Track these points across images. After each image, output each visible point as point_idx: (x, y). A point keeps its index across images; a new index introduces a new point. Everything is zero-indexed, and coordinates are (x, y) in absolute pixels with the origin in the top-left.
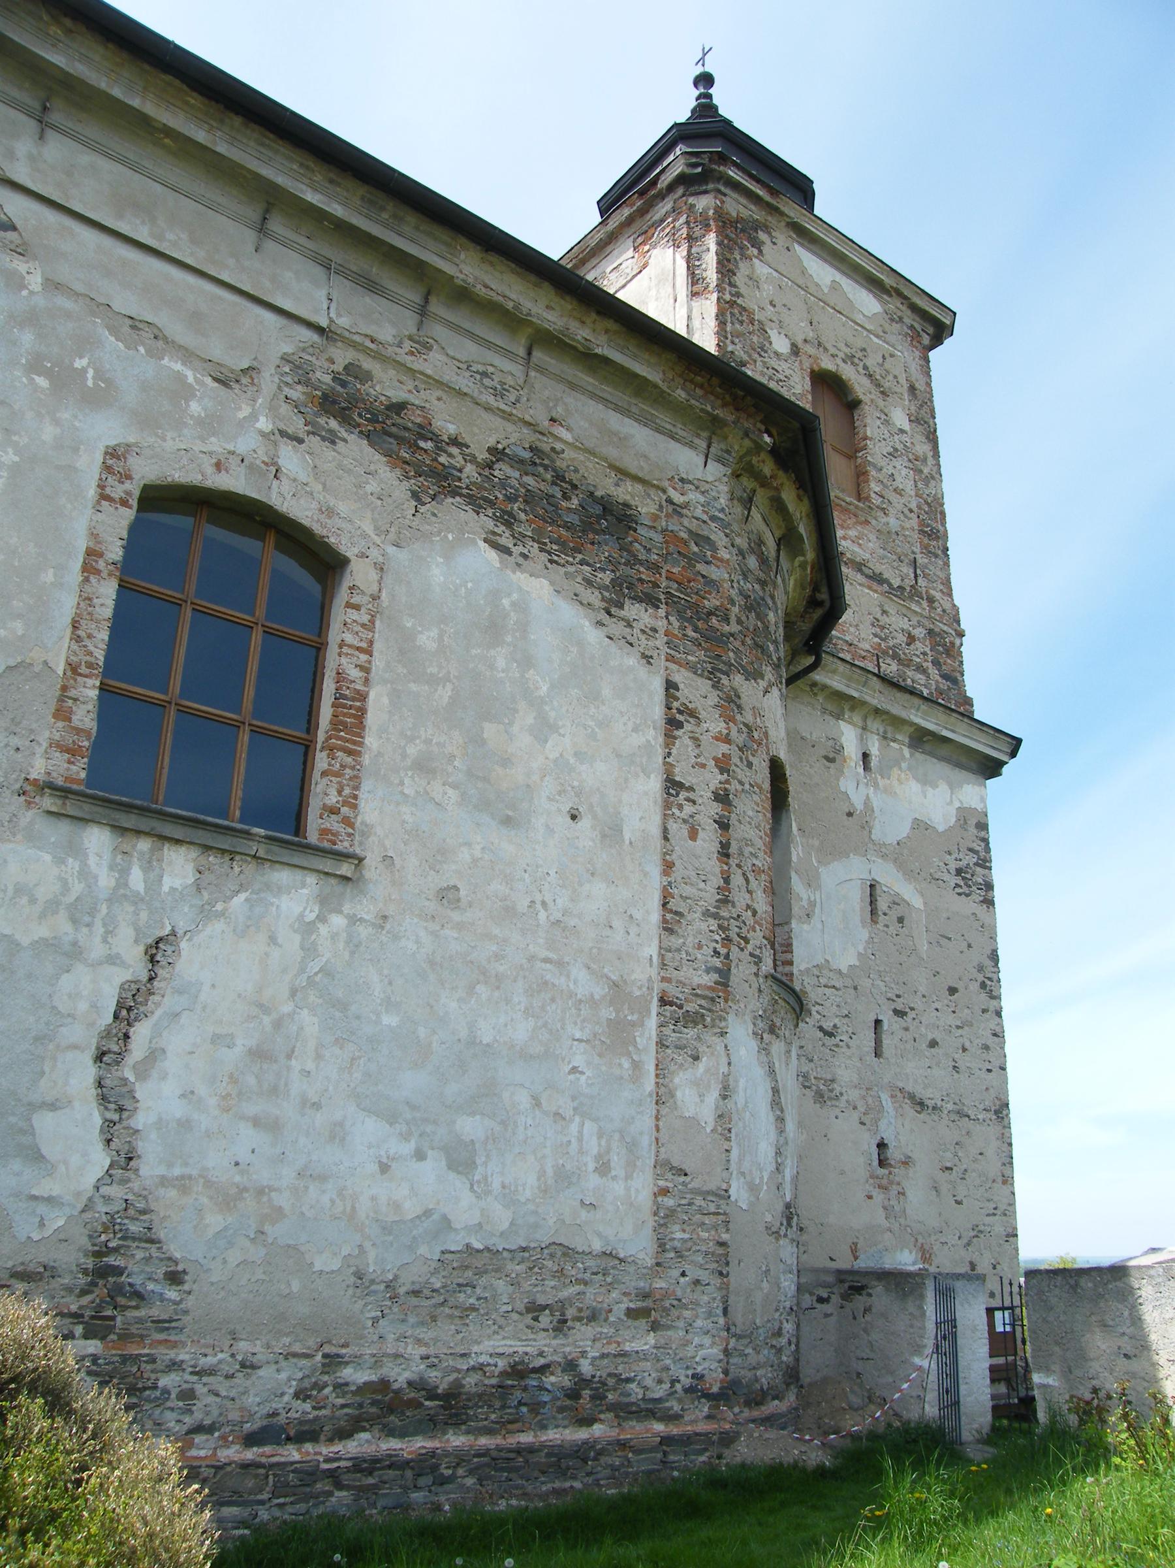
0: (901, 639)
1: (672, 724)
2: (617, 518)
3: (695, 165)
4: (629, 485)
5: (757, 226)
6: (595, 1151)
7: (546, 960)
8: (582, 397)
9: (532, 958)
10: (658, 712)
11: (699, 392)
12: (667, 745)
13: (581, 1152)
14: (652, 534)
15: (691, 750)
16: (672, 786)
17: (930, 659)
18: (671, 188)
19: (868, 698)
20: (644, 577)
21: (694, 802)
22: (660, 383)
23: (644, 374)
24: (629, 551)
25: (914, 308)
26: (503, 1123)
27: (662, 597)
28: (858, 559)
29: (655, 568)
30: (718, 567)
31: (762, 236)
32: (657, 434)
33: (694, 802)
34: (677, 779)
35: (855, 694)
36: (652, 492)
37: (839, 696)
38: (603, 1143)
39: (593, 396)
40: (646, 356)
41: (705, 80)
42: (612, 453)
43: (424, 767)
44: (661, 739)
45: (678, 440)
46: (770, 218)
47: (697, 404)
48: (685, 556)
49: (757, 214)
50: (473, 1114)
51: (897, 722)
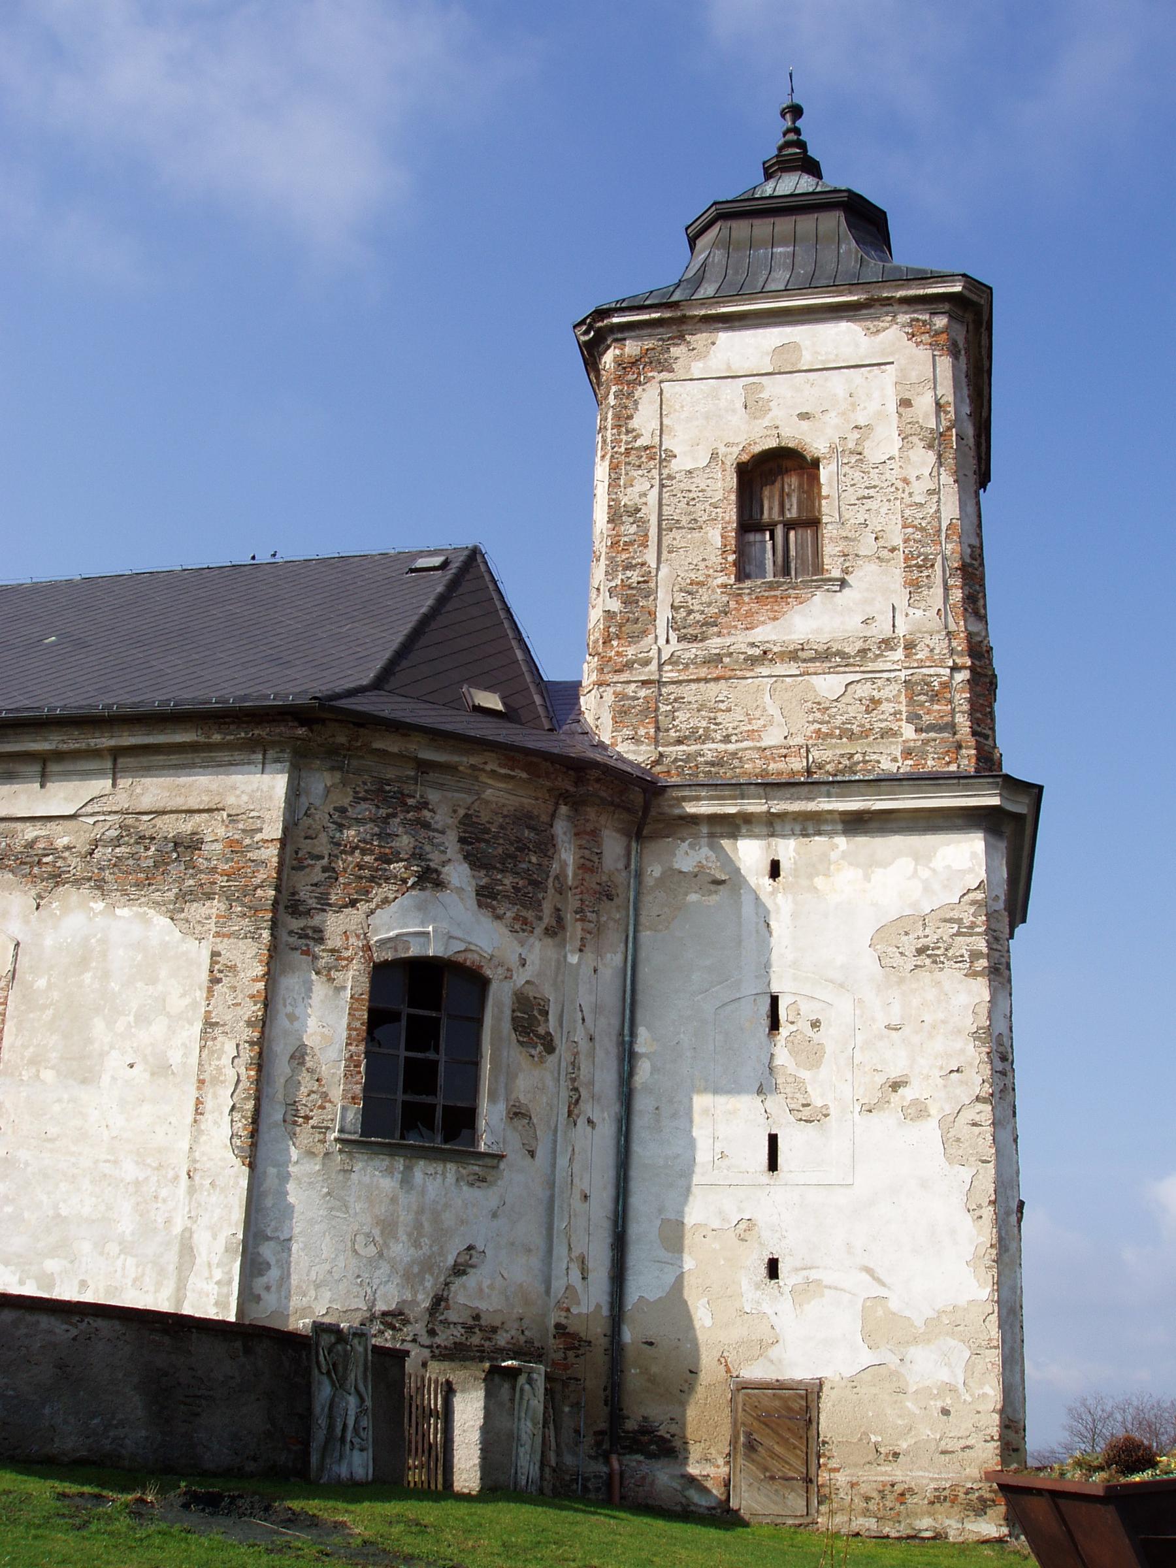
0: (855, 710)
1: (215, 981)
4: (197, 818)
6: (134, 1276)
7: (107, 1161)
9: (96, 1162)
10: (204, 976)
11: (232, 727)
13: (123, 1276)
16: (209, 1024)
26: (72, 1262)
28: (791, 648)
29: (214, 870)
37: (713, 819)
38: (140, 1270)
41: (796, 111)
43: (34, 1061)
45: (237, 765)
50: (53, 1258)
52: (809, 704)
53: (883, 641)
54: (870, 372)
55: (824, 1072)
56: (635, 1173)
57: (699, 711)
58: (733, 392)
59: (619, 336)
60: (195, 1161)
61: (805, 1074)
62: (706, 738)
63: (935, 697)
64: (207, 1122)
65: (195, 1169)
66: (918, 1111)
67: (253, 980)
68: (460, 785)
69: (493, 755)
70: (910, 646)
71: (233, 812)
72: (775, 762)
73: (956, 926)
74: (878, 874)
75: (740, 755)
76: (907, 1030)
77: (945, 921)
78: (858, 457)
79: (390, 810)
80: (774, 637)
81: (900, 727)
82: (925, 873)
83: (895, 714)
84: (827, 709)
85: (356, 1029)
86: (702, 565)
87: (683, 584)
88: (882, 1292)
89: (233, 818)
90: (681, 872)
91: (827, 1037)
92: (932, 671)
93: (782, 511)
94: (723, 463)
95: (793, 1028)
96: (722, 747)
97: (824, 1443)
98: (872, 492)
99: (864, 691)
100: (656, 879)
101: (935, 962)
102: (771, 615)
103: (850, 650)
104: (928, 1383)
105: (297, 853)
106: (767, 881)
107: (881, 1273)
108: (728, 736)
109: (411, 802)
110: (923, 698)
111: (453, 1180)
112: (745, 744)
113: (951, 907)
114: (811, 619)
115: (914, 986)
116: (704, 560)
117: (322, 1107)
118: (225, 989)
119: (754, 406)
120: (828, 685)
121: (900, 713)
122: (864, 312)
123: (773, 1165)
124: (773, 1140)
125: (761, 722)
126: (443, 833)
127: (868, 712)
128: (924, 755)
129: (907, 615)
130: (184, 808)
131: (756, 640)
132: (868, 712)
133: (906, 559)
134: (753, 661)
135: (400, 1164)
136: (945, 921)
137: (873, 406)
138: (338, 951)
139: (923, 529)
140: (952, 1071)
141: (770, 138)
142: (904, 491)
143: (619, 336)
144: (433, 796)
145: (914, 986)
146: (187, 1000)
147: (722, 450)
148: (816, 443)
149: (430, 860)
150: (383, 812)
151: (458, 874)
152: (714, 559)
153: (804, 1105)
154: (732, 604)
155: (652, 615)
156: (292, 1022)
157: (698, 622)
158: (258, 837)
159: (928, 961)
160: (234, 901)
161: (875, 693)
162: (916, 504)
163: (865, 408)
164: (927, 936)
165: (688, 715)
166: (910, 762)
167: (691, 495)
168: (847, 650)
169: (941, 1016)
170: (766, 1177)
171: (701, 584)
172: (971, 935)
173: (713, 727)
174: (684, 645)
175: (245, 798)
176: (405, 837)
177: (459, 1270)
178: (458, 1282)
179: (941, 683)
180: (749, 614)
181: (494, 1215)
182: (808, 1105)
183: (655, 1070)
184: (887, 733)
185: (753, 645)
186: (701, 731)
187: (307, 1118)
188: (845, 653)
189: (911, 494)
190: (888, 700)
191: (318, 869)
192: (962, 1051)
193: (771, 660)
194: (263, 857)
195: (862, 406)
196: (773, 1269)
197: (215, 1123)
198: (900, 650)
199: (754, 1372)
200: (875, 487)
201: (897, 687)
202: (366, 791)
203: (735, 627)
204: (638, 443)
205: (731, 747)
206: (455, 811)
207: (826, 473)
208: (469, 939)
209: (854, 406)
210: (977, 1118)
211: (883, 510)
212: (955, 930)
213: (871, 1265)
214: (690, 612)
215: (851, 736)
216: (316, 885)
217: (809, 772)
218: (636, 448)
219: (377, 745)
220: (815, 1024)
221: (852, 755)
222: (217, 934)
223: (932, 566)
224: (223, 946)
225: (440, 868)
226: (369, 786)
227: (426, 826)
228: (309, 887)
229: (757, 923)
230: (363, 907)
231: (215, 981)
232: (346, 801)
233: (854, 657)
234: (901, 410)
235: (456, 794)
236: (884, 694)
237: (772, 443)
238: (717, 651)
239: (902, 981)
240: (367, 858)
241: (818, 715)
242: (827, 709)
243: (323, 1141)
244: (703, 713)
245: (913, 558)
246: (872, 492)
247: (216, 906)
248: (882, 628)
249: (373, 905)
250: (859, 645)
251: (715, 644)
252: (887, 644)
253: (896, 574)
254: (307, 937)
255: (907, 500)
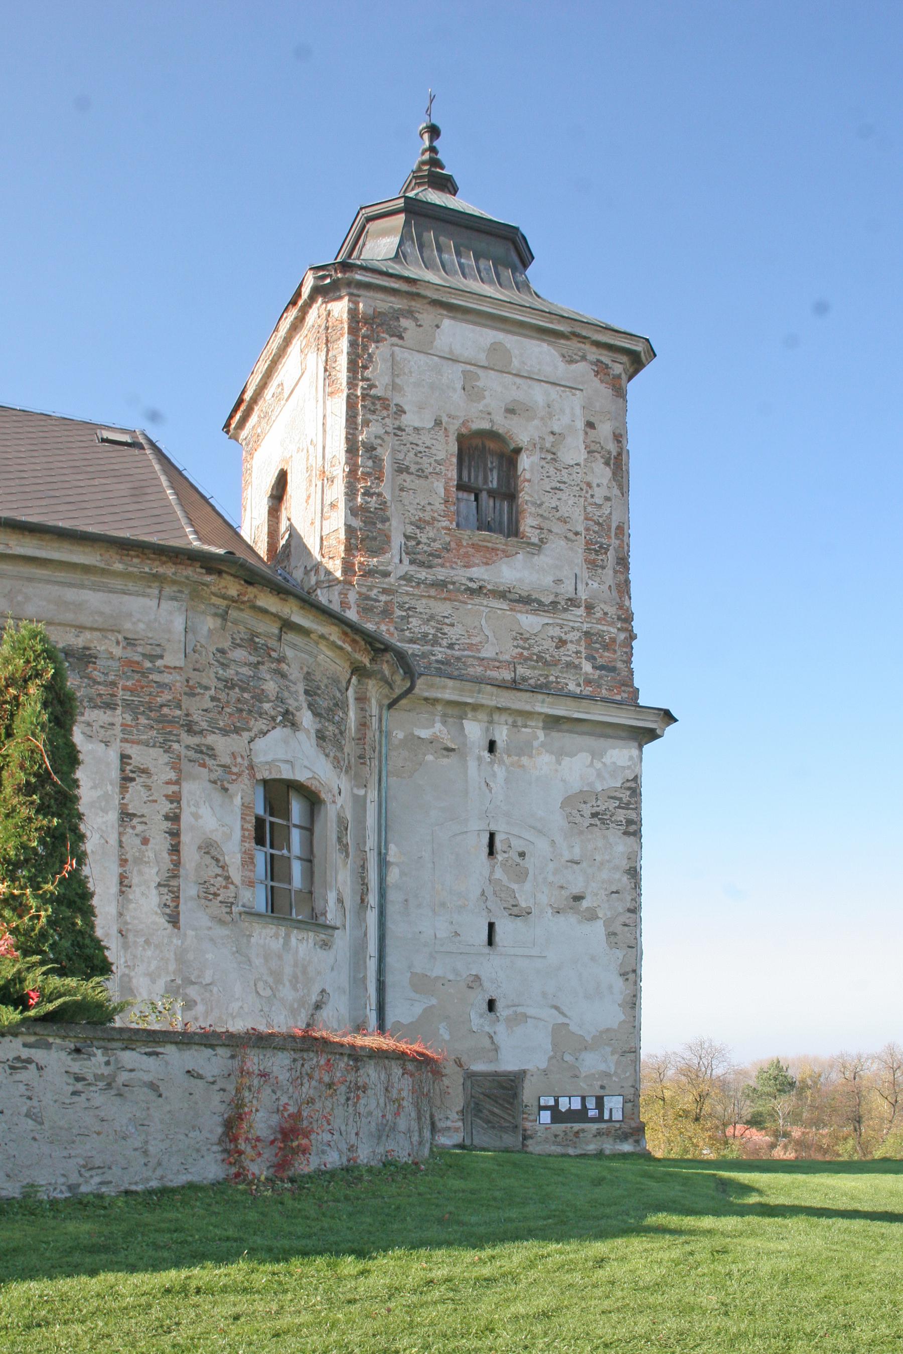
0: (549, 645)
1: (126, 780)
2: (78, 659)
3: (323, 277)
4: (88, 635)
5: (397, 315)
8: (40, 585)
10: (115, 774)
12: (121, 793)
14: (110, 662)
15: (144, 793)
16: (126, 816)
17: (583, 655)
18: (312, 299)
19: (484, 702)
20: (102, 692)
21: (146, 823)
22: (98, 564)
23: (82, 561)
24: (89, 678)
25: (598, 344)
27: (119, 702)
28: (501, 588)
29: (113, 684)
30: (171, 673)
31: (404, 322)
32: (110, 595)
33: (146, 823)
34: (130, 812)
35: (469, 700)
36: (109, 635)
39: (48, 582)
40: (81, 549)
42: (69, 617)
44: (117, 790)
45: (130, 594)
46: (413, 303)
47: (136, 569)
48: (138, 672)
49: (398, 303)
51: (528, 715)
52: (514, 633)
53: (569, 599)
54: (563, 391)
55: (528, 886)
56: (389, 942)
57: (428, 620)
58: (453, 374)
59: (355, 291)
60: (126, 923)
61: (515, 886)
62: (435, 642)
63: (606, 647)
64: (135, 894)
65: (128, 930)
66: (591, 916)
67: (167, 783)
68: (307, 647)
69: (337, 629)
70: (590, 608)
71: (129, 636)
72: (491, 670)
73: (618, 802)
74: (566, 761)
75: (463, 660)
76: (584, 865)
77: (612, 798)
78: (552, 456)
79: (260, 659)
80: (486, 577)
81: (580, 663)
82: (598, 765)
83: (577, 653)
84: (528, 639)
85: (248, 830)
86: (428, 508)
87: (413, 519)
88: (566, 1021)
89: (130, 642)
90: (420, 738)
91: (529, 863)
92: (605, 628)
93: (485, 481)
94: (446, 429)
95: (506, 855)
96: (449, 652)
97: (526, 1106)
98: (562, 486)
99: (556, 632)
100: (401, 740)
101: (604, 824)
102: (485, 560)
103: (547, 600)
104: (593, 1071)
105: (187, 681)
106: (486, 754)
107: (565, 1009)
108: (452, 644)
109: (274, 654)
110: (597, 646)
111: (312, 945)
112: (466, 653)
113: (616, 789)
114: (514, 571)
115: (590, 837)
116: (429, 504)
117: (226, 887)
118: (139, 787)
119: (471, 390)
120: (530, 622)
121: (580, 652)
122: (562, 341)
123: (490, 942)
124: (491, 926)
125: (478, 639)
126: (295, 684)
127: (557, 648)
128: (600, 686)
129: (587, 584)
130: (74, 623)
131: (474, 576)
132: (557, 648)
133: (587, 543)
134: (472, 592)
135: (282, 931)
136: (612, 798)
137: (566, 420)
138: (229, 767)
139: (599, 524)
140: (613, 892)
141: (414, 155)
142: (587, 492)
143: (355, 291)
144: (289, 653)
145: (590, 837)
146: (99, 792)
147: (445, 419)
148: (522, 433)
149: (290, 705)
150: (253, 659)
151: (306, 718)
152: (438, 506)
153: (513, 906)
154: (453, 545)
155: (387, 539)
156: (196, 820)
157: (425, 552)
158: (159, 663)
159: (598, 823)
160: (140, 714)
161: (563, 635)
162: (596, 504)
163: (559, 420)
164: (598, 806)
165: (420, 622)
166: (591, 689)
167: (419, 449)
168: (543, 600)
169: (607, 857)
170: (487, 950)
171: (428, 523)
172: (628, 809)
173: (440, 635)
174: (413, 568)
175: (141, 626)
176: (271, 682)
177: (318, 1007)
178: (318, 1012)
179: (610, 638)
180: (466, 555)
181: (332, 969)
182: (516, 906)
183: (403, 874)
184: (569, 665)
185: (471, 580)
186: (430, 637)
187: (216, 895)
188: (541, 601)
189: (592, 496)
190: (571, 642)
191: (207, 697)
192: (620, 880)
193: (486, 594)
194: (166, 681)
195: (557, 417)
196: (491, 1005)
197: (143, 894)
198: (582, 608)
199: (479, 1067)
200: (565, 483)
201: (579, 634)
202: (241, 639)
203: (456, 563)
204: (373, 392)
205: (457, 653)
206: (302, 668)
207: (525, 462)
208: (316, 771)
209: (551, 416)
210: (627, 922)
211: (570, 502)
212: (617, 805)
213: (559, 1005)
214: (419, 543)
215: (546, 663)
216: (206, 710)
217: (514, 681)
218: (370, 396)
219: (260, 603)
220: (522, 855)
221: (547, 676)
222: (124, 740)
223: (606, 553)
224: (132, 750)
225: (295, 712)
226: (242, 636)
227: (283, 676)
228: (200, 712)
229: (480, 783)
230: (246, 735)
231: (126, 780)
232: (226, 644)
233: (547, 606)
234: (588, 430)
235: (303, 655)
236: (569, 637)
237: (485, 425)
238: (443, 578)
239: (581, 833)
240: (246, 695)
241: (521, 643)
242: (528, 639)
243: (230, 913)
244: (432, 623)
245: (592, 544)
246: (562, 486)
247: (119, 717)
248: (567, 589)
249: (252, 734)
250: (551, 598)
251: (441, 573)
252: (573, 602)
253: (578, 554)
254: (201, 752)
255: (590, 500)
